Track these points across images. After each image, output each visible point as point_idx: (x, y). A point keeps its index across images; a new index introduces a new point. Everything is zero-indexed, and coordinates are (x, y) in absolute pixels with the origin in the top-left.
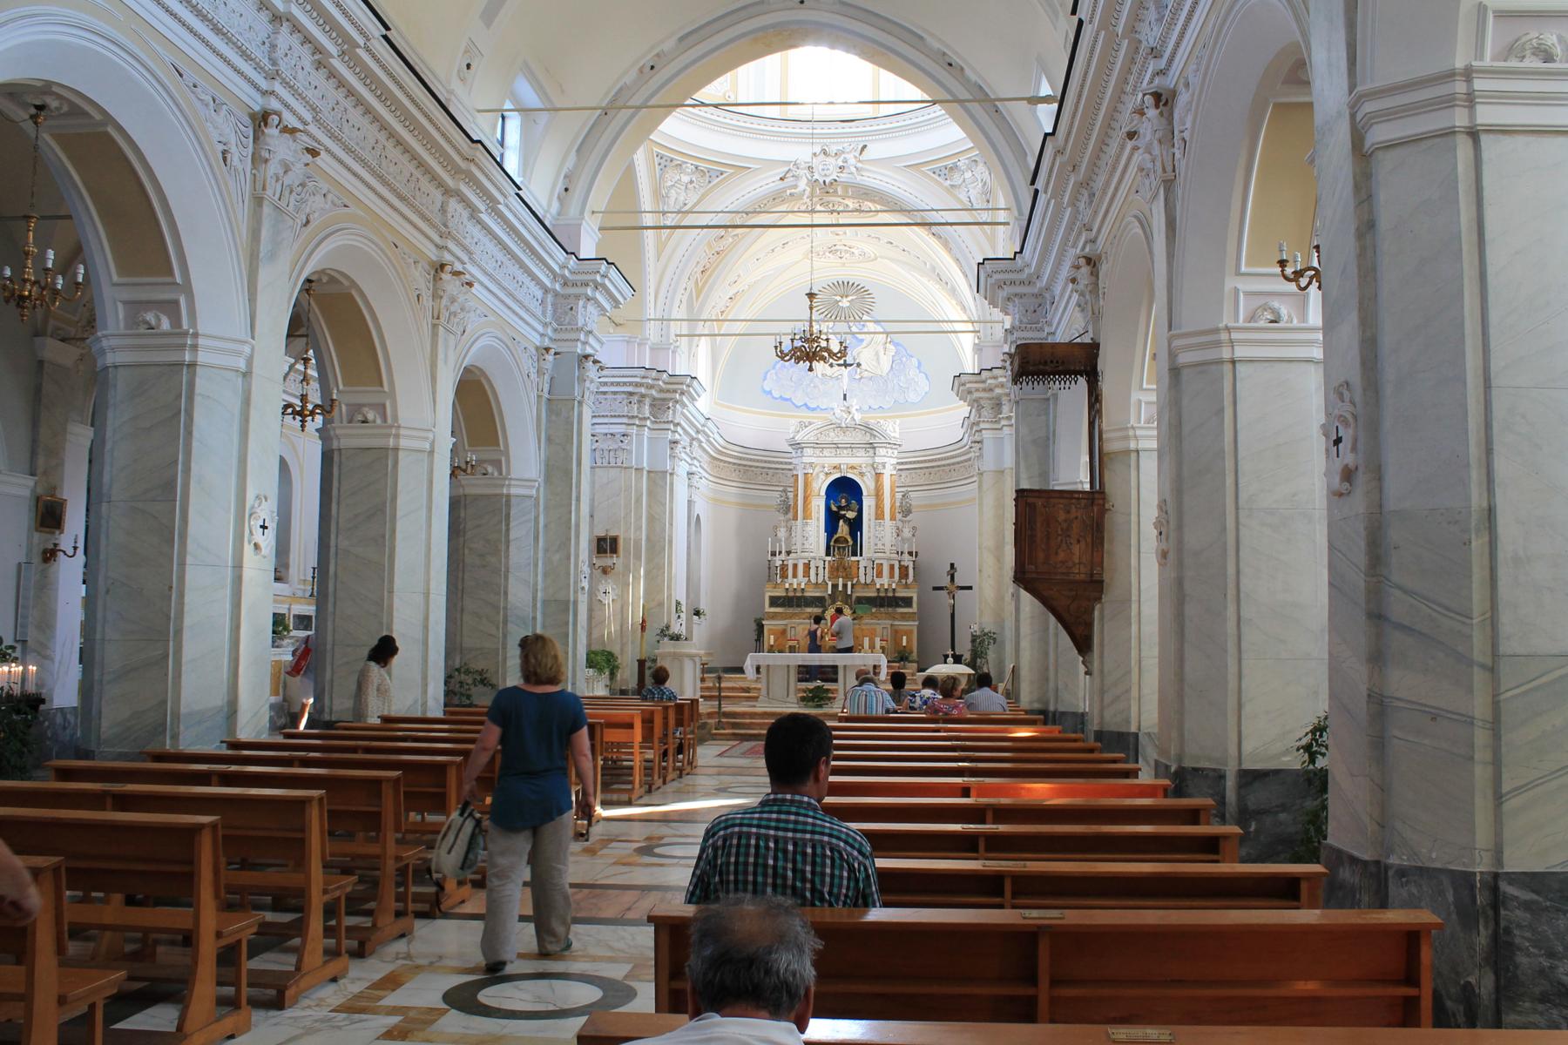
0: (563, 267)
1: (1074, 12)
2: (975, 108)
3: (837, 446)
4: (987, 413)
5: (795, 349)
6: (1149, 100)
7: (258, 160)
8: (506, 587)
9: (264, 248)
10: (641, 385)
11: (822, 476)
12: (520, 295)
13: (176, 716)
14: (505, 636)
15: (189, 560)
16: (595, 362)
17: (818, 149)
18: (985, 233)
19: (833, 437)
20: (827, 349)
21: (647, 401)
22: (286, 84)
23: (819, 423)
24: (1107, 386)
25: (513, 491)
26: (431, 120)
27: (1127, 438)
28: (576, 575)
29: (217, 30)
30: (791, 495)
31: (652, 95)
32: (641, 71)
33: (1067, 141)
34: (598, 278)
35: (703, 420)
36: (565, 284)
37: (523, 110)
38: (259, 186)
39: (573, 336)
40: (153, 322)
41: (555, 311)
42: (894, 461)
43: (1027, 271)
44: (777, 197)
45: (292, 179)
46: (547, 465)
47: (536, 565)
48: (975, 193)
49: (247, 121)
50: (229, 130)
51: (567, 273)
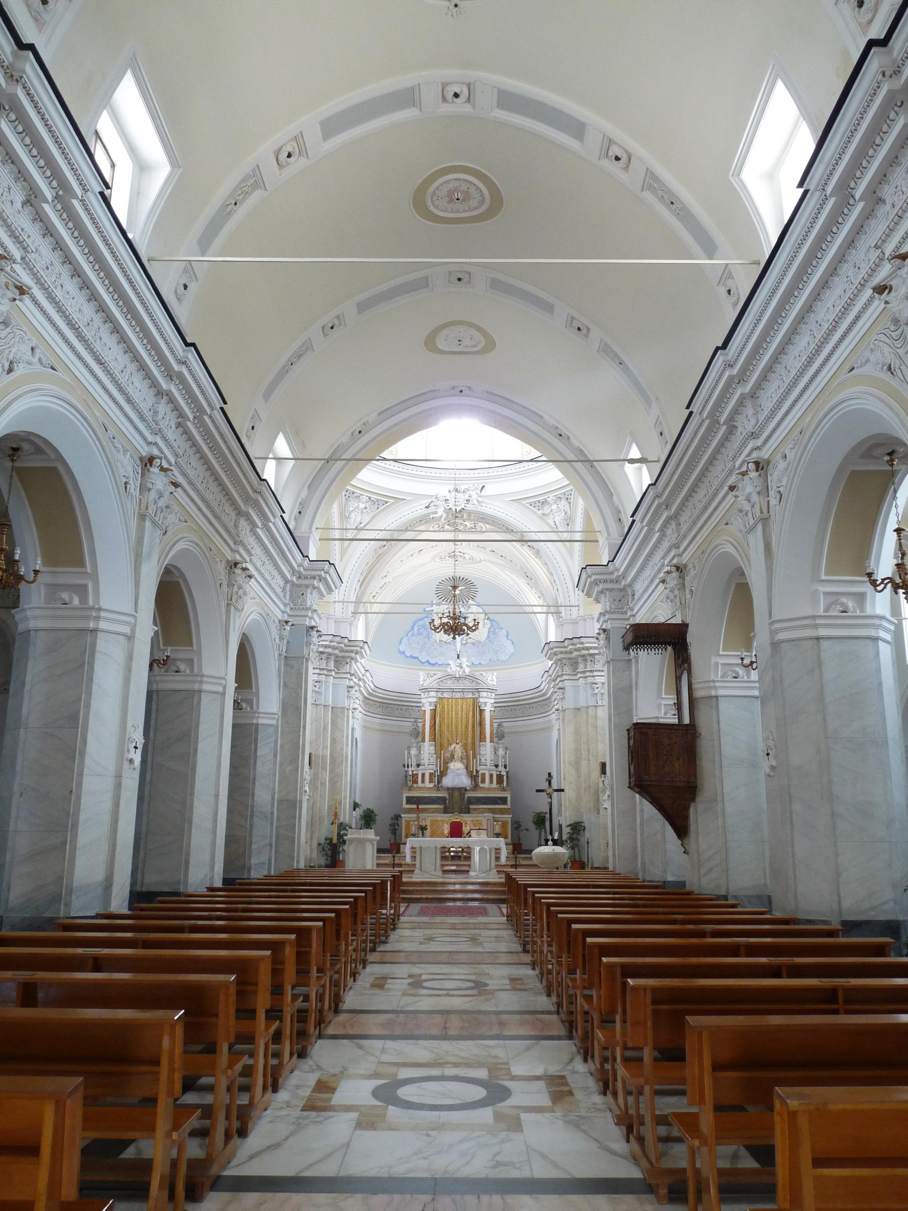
0: (300, 565)
1: (688, 407)
2: (579, 465)
4: (567, 670)
5: (443, 625)
6: (752, 466)
7: (144, 489)
8: (253, 790)
9: (145, 549)
10: (337, 648)
12: (273, 583)
13: (70, 890)
14: (251, 826)
15: (86, 771)
16: (318, 631)
17: (452, 488)
18: (565, 546)
20: (466, 625)
21: (333, 658)
22: (164, 438)
23: (439, 674)
24: (695, 652)
25: (261, 721)
26: (239, 465)
28: (302, 782)
29: (129, 401)
30: (420, 725)
33: (665, 489)
34: (322, 573)
35: (363, 671)
36: (299, 577)
37: (278, 459)
38: (143, 506)
40: (67, 600)
41: (291, 596)
42: (493, 701)
43: (616, 574)
44: (423, 520)
45: (162, 503)
46: (283, 703)
47: (275, 775)
48: (559, 518)
49: (139, 462)
50: (128, 467)
51: (302, 570)
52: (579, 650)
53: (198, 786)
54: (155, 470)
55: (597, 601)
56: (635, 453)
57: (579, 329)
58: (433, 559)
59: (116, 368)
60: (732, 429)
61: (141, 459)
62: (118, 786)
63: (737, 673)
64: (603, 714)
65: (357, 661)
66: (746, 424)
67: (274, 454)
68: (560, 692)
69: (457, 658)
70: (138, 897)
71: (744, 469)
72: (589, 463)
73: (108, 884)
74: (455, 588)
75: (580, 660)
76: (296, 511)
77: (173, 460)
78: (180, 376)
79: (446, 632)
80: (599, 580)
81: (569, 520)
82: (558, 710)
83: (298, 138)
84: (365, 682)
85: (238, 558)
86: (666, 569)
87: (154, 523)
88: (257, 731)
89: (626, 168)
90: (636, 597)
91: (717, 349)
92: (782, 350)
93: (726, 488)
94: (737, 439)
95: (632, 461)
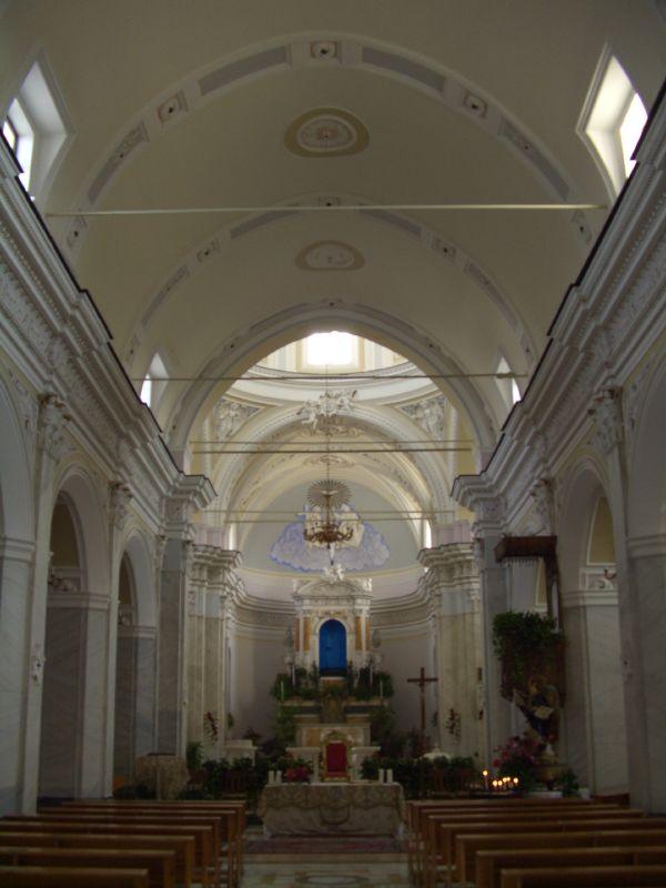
0: (175, 481)
1: (549, 334)
2: (454, 381)
3: (327, 598)
4: (443, 576)
6: (607, 394)
7: (41, 424)
9: (43, 481)
11: (317, 619)
12: (150, 499)
17: (323, 393)
19: (324, 591)
20: (338, 533)
22: (59, 377)
23: (314, 581)
24: (563, 564)
27: (577, 598)
29: (30, 346)
30: (294, 633)
31: (228, 369)
32: (225, 348)
34: (198, 488)
37: (154, 379)
39: (177, 528)
42: (367, 608)
44: (295, 426)
45: (56, 435)
47: (155, 687)
48: (432, 422)
50: (28, 406)
52: (455, 556)
53: (88, 701)
54: (51, 407)
55: (471, 509)
56: (504, 368)
57: (446, 250)
58: (305, 463)
59: (19, 318)
60: (589, 357)
61: (39, 397)
62: (25, 701)
63: (603, 583)
64: (478, 620)
65: (230, 571)
66: (601, 353)
67: (151, 374)
68: (436, 599)
69: (332, 565)
70: (43, 802)
71: (601, 395)
72: (462, 376)
73: (20, 789)
74: (328, 494)
75: (456, 566)
76: (171, 425)
77: (65, 395)
78: (74, 320)
79: (321, 541)
80: (470, 489)
81: (442, 425)
82: (434, 616)
83: (179, 96)
84: (237, 591)
85: (120, 479)
86: (536, 482)
87: (50, 455)
88: (136, 645)
89: (483, 115)
90: (509, 507)
91: (571, 286)
92: (628, 291)
93: (585, 412)
94: (592, 370)
95: (501, 376)
